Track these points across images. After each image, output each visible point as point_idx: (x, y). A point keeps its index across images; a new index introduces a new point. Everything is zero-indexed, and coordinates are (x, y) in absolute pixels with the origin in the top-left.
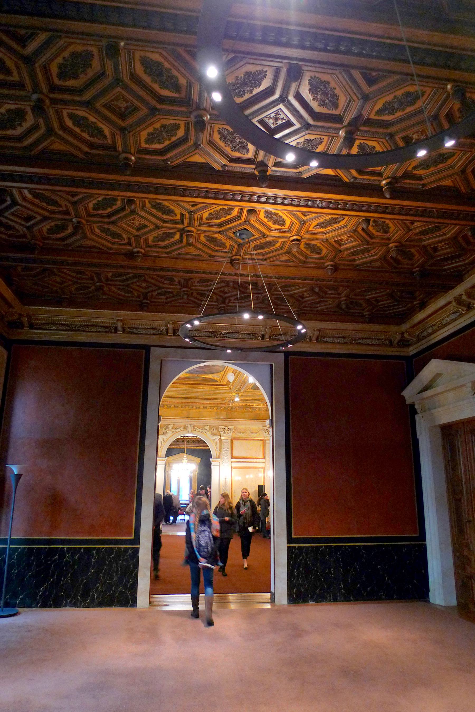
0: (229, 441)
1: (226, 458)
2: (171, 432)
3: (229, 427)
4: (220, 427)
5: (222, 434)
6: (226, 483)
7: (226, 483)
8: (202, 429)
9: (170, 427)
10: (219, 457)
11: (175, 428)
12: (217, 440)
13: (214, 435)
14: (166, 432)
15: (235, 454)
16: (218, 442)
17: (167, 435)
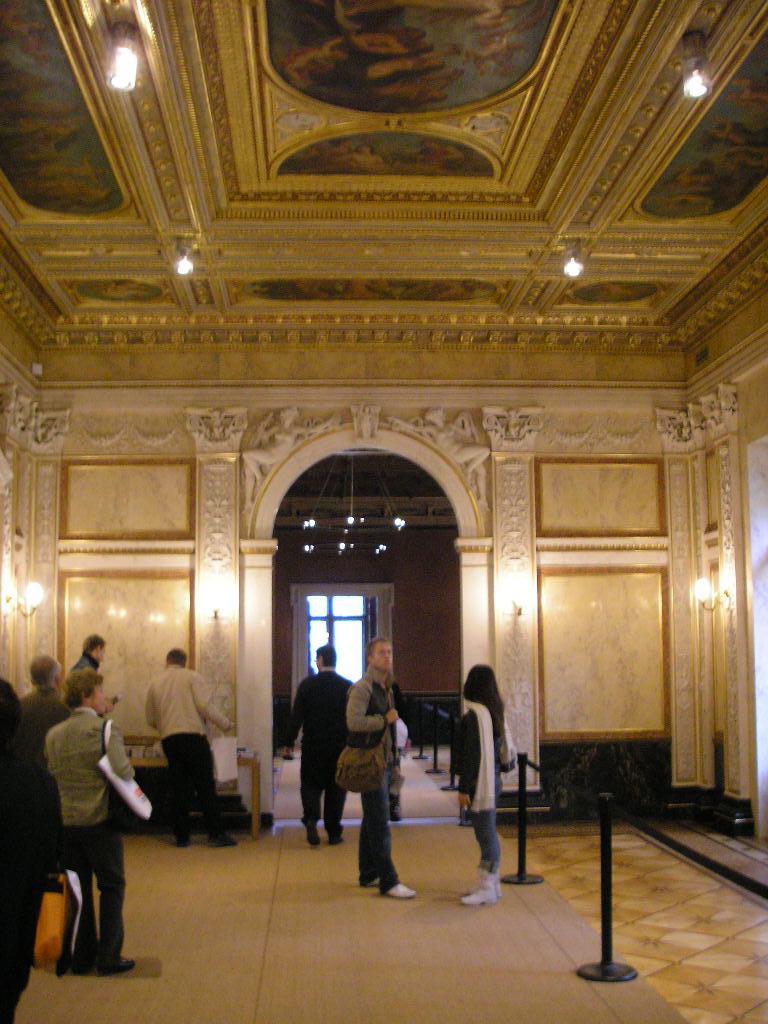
0: (526, 468)
2: (289, 440)
3: (529, 411)
4: (487, 410)
5: (495, 438)
6: (516, 631)
7: (516, 631)
8: (416, 424)
9: (289, 417)
10: (189, 535)
11: (307, 421)
12: (478, 465)
13: (466, 444)
14: (272, 439)
15: (548, 522)
16: (482, 472)
17: (274, 451)
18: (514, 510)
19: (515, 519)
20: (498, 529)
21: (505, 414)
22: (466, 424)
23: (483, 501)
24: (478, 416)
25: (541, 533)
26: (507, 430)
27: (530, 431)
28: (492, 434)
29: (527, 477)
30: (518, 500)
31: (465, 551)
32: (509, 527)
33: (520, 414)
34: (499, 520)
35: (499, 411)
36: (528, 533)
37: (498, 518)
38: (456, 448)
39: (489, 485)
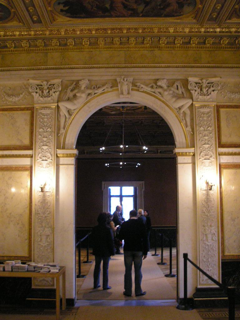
1: (207, 146)
4: (190, 79)
5: (195, 94)
12: (186, 109)
13: (179, 97)
15: (224, 140)
16: (188, 112)
18: (206, 132)
19: (206, 138)
20: (198, 143)
21: (200, 81)
22: (179, 87)
23: (189, 129)
24: (185, 83)
25: (221, 146)
26: (201, 90)
27: (213, 91)
28: (193, 92)
29: (212, 115)
30: (208, 127)
31: (180, 155)
32: (203, 142)
33: (208, 81)
34: (198, 138)
35: (196, 80)
36: (214, 145)
37: (198, 137)
38: (174, 99)
39: (192, 119)
